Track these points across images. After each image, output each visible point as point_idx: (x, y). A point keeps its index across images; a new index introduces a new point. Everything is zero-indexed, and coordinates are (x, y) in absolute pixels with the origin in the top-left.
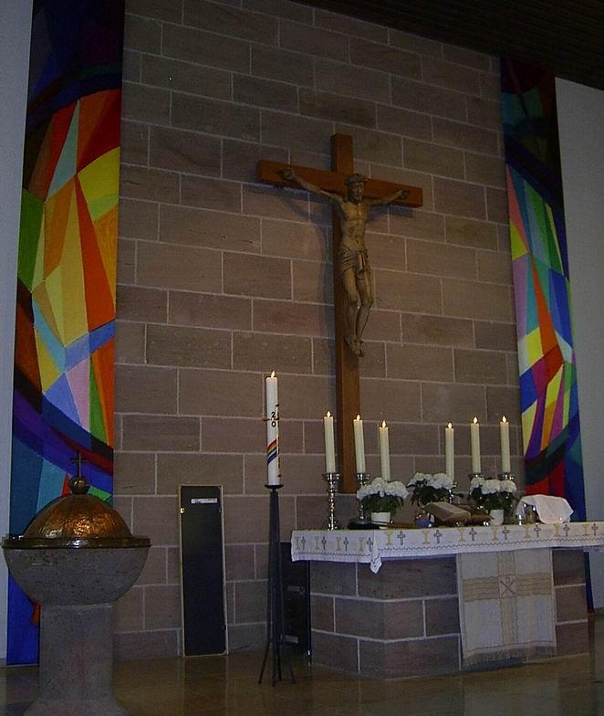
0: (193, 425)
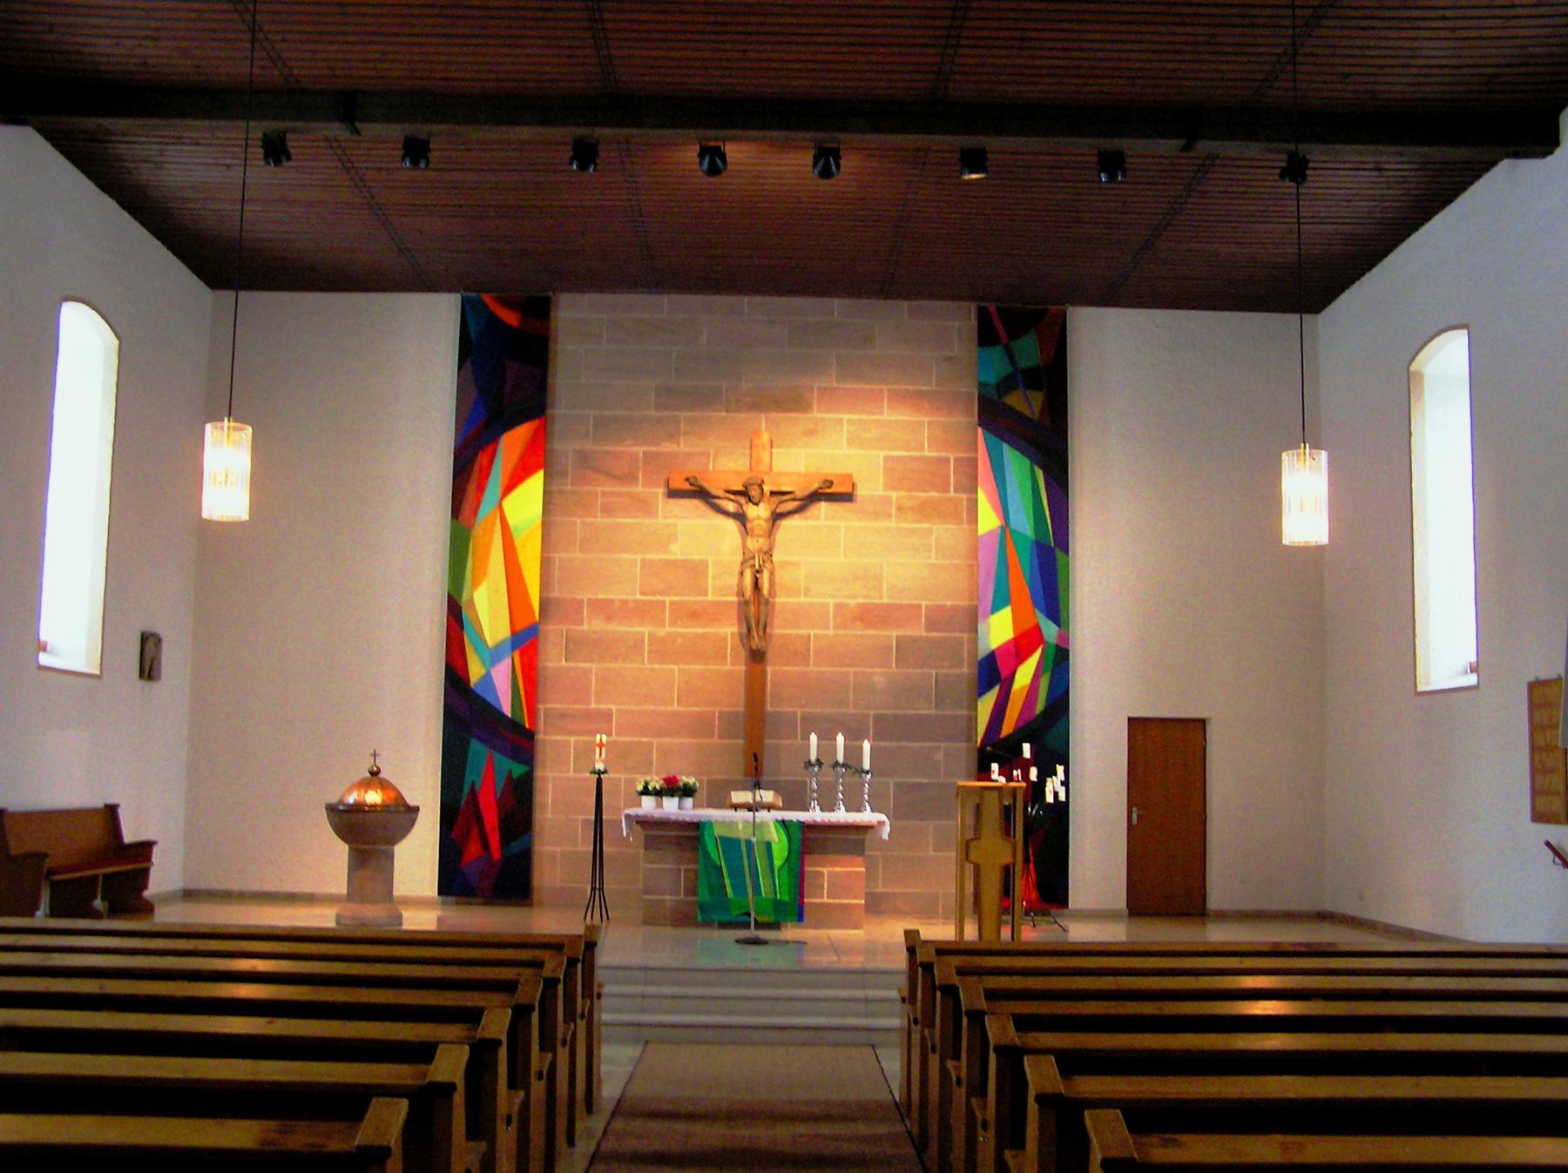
0: (607, 716)
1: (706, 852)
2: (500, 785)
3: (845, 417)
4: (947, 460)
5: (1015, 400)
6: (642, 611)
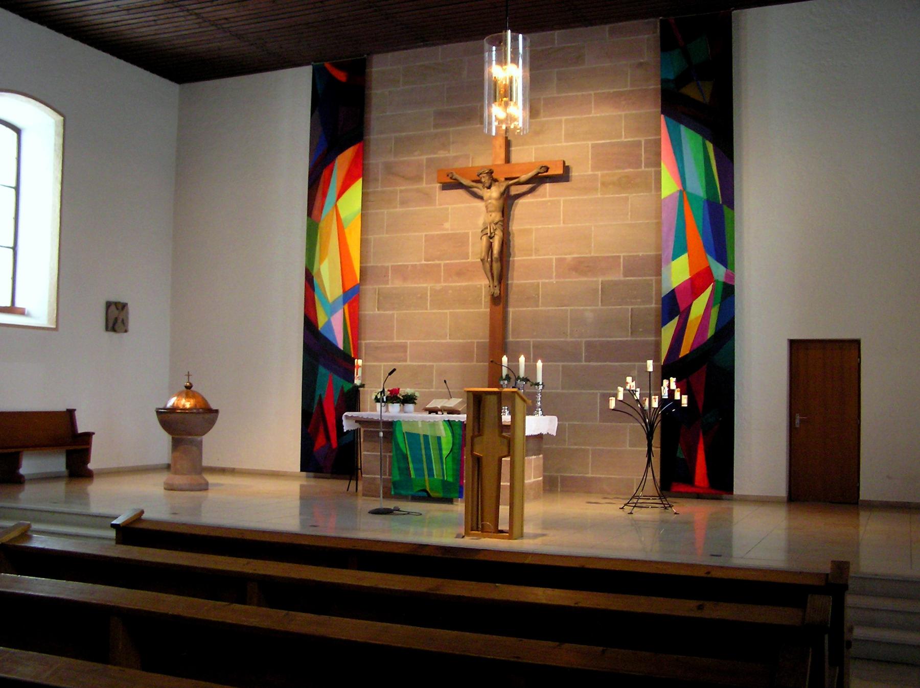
0: (403, 347)
1: (397, 445)
2: (336, 396)
3: (564, 118)
4: (640, 142)
5: (690, 91)
6: (427, 272)
